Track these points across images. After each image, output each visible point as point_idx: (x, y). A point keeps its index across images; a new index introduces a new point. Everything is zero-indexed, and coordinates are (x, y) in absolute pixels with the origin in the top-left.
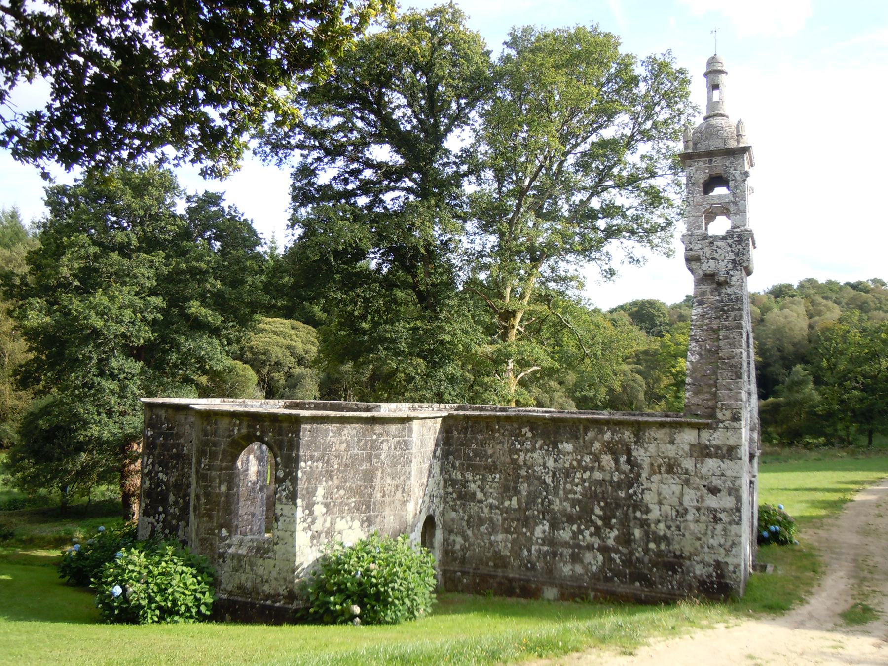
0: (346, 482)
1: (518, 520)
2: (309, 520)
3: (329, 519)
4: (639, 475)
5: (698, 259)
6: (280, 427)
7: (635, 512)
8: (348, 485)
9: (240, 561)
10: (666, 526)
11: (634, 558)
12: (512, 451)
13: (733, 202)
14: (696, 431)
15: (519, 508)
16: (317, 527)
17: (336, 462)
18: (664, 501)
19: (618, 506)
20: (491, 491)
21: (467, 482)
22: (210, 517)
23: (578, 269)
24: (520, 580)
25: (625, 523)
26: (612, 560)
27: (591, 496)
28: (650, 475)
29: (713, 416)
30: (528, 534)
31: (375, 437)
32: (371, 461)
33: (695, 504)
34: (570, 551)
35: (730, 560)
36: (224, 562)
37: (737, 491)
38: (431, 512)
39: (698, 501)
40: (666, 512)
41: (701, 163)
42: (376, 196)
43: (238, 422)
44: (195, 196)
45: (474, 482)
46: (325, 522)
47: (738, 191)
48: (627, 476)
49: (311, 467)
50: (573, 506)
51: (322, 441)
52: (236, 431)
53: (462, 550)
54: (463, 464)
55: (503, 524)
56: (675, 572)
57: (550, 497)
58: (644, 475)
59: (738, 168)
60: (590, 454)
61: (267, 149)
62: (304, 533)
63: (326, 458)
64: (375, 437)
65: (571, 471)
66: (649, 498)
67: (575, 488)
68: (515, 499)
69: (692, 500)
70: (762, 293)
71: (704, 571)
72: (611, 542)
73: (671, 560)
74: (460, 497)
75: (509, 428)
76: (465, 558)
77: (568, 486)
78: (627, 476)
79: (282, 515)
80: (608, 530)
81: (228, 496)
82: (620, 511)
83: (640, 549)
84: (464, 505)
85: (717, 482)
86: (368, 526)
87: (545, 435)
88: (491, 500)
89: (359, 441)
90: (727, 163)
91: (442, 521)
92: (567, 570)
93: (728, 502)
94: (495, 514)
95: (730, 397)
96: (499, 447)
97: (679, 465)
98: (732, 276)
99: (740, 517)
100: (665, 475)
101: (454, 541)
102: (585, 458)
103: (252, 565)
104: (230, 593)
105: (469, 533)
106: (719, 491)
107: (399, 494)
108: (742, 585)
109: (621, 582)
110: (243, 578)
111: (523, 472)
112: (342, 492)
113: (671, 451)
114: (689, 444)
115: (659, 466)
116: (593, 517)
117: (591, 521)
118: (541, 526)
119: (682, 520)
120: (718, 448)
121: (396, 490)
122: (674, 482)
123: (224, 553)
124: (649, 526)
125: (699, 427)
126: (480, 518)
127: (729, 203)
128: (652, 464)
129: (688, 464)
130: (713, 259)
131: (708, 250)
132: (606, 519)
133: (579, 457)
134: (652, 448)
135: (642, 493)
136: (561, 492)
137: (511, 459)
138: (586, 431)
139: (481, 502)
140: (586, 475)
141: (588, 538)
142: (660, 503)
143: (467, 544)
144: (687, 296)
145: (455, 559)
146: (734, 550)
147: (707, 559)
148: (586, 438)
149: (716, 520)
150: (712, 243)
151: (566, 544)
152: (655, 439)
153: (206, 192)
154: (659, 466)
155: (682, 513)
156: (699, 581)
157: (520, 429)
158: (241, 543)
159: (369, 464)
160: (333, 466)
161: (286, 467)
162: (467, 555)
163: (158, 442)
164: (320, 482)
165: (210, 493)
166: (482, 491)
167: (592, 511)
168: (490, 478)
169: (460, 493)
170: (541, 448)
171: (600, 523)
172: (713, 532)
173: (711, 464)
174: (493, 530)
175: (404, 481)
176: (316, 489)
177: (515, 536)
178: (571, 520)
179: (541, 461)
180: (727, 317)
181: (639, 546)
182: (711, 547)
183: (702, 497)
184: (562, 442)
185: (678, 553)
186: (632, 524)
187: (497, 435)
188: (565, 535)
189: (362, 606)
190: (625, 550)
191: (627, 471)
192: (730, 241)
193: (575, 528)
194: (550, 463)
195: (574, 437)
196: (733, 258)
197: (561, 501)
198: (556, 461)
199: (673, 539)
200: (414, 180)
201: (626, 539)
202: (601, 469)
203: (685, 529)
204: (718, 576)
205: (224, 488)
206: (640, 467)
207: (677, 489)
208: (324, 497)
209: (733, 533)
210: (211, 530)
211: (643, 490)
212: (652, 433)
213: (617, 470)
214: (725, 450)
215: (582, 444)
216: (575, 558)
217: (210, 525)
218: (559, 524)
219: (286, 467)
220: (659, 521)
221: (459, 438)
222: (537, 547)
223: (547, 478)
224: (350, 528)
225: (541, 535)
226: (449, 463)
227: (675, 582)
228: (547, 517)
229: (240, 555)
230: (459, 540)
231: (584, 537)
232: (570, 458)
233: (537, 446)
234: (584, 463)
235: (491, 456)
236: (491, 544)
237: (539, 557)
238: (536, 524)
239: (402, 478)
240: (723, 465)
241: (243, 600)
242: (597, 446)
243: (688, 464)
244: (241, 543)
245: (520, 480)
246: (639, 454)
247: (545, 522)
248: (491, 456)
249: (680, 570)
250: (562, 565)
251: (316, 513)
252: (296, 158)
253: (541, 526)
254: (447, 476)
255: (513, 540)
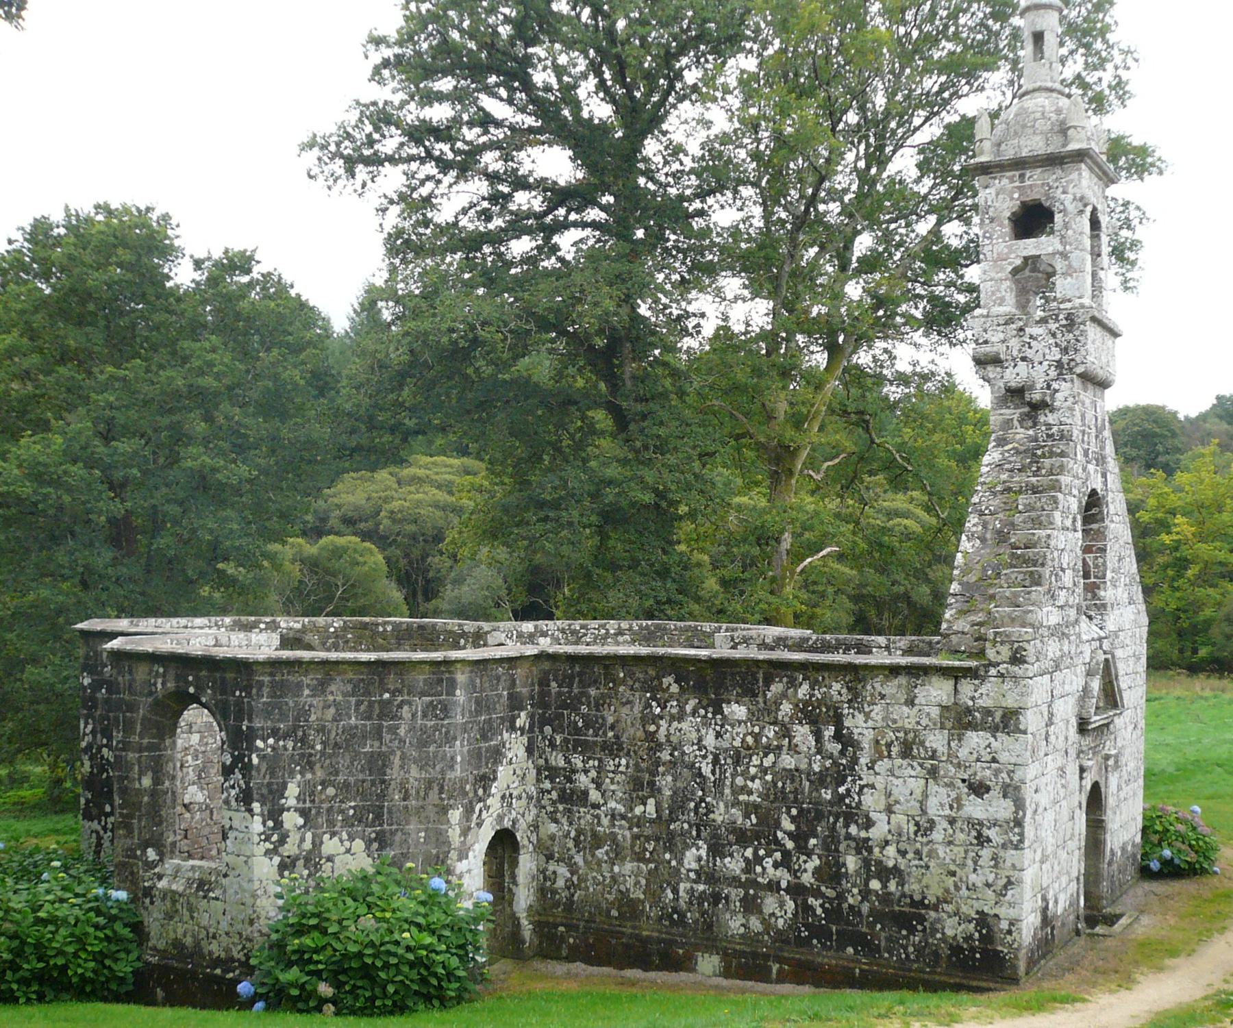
0: (337, 773)
1: (657, 839)
2: (275, 838)
3: (309, 836)
4: (855, 761)
5: (996, 361)
6: (223, 680)
7: (847, 826)
8: (341, 778)
9: (174, 902)
10: (899, 851)
11: (845, 906)
12: (648, 718)
13: (1061, 254)
14: (952, 682)
15: (659, 817)
16: (290, 848)
17: (318, 740)
18: (897, 808)
19: (820, 816)
20: (613, 787)
21: (574, 771)
22: (128, 827)
23: (938, 360)
24: (659, 941)
25: (831, 845)
26: (809, 909)
27: (776, 798)
28: (873, 762)
29: (981, 654)
30: (674, 863)
31: (387, 696)
32: (380, 738)
33: (948, 812)
34: (742, 892)
35: (1002, 911)
36: (152, 903)
37: (1017, 788)
38: (507, 824)
39: (951, 807)
40: (900, 827)
41: (1005, 181)
42: (547, 239)
43: (161, 670)
44: (209, 259)
45: (586, 771)
46: (303, 840)
47: (1070, 232)
48: (835, 763)
49: (274, 749)
50: (747, 816)
51: (291, 704)
52: (159, 686)
53: (569, 888)
54: (566, 741)
55: (633, 846)
56: (912, 931)
57: (708, 799)
58: (863, 761)
59: (1070, 190)
60: (775, 723)
61: (338, 166)
62: (267, 860)
63: (300, 733)
64: (387, 696)
65: (743, 752)
66: (870, 801)
67: (750, 784)
68: (651, 801)
69: (942, 805)
70: (1181, 417)
71: (960, 929)
72: (807, 879)
73: (906, 909)
74: (564, 797)
75: (641, 676)
76: (572, 902)
77: (739, 781)
78: (835, 763)
79: (231, 828)
80: (804, 858)
81: (154, 793)
82: (824, 824)
83: (855, 891)
84: (570, 811)
85: (983, 773)
86: (381, 848)
87: (700, 688)
88: (612, 804)
89: (358, 704)
90: (1051, 180)
91: (534, 838)
92: (735, 924)
93: (1001, 808)
94: (621, 827)
95: (1013, 620)
96: (625, 710)
97: (922, 743)
98: (1056, 391)
99: (1022, 834)
100: (899, 761)
101: (554, 872)
102: (766, 730)
103: (191, 910)
104: (163, 954)
105: (579, 859)
106: (988, 789)
107: (433, 796)
108: (1022, 954)
109: (824, 945)
110: (180, 931)
111: (665, 756)
112: (331, 791)
113: (906, 717)
114: (940, 705)
115: (889, 745)
116: (780, 834)
117: (777, 841)
118: (694, 850)
119: (925, 840)
120: (988, 712)
121: (429, 787)
122: (913, 773)
123: (151, 888)
124: (870, 850)
125: (955, 675)
126: (595, 835)
127: (1053, 254)
128: (877, 742)
129: (937, 740)
130: (1024, 359)
131: (1014, 343)
132: (800, 838)
133: (757, 729)
134: (877, 712)
135: (860, 793)
136: (727, 791)
137: (646, 732)
138: (768, 682)
139: (596, 806)
140: (768, 761)
141: (770, 870)
142: (889, 810)
143: (575, 879)
144: (1218, 398)
145: (557, 904)
146: (1010, 893)
147: (964, 909)
148: (769, 695)
149: (982, 840)
150: (1021, 329)
151: (734, 881)
152: (883, 697)
153: (226, 251)
154: (889, 745)
155: (925, 828)
156: (951, 947)
157: (659, 678)
158: (177, 872)
159: (377, 744)
160: (313, 747)
161: (234, 749)
162: (576, 898)
163: (99, 695)
164: (292, 774)
165: (126, 788)
166: (598, 787)
167: (778, 825)
168: (610, 764)
169: (563, 790)
170: (694, 712)
171: (790, 845)
172: (975, 863)
173: (975, 740)
174: (617, 854)
175: (443, 772)
176: (284, 786)
177: (652, 866)
178: (743, 838)
179: (694, 736)
180: (1039, 469)
181: (854, 886)
182: (972, 888)
183: (958, 799)
184: (729, 702)
185: (917, 897)
186: (842, 848)
187: (621, 689)
188: (733, 865)
189: (338, 985)
190: (830, 893)
191: (836, 753)
192: (1053, 326)
193: (749, 853)
194: (710, 740)
195: (749, 692)
196: (1058, 357)
197: (726, 807)
198: (718, 735)
199: (909, 874)
200: (603, 208)
201: (831, 873)
202: (793, 749)
203: (929, 855)
204: (982, 938)
205: (147, 782)
206: (856, 745)
207: (917, 785)
208: (298, 798)
209: (1008, 864)
210: (131, 850)
211: (862, 788)
212: (877, 685)
213: (819, 752)
214: (998, 716)
215: (762, 705)
216: (750, 906)
217: (129, 841)
218: (723, 846)
219: (234, 749)
220: (887, 843)
221: (559, 694)
222: (688, 885)
223: (703, 765)
224: (348, 851)
225: (694, 866)
226: (544, 738)
227: (911, 949)
228: (703, 834)
229: (174, 892)
230: (563, 871)
231: (764, 869)
232: (741, 730)
233: (689, 708)
234: (764, 740)
235: (612, 728)
236: (614, 879)
237: (691, 903)
238: (687, 847)
239: (438, 768)
240: (995, 744)
241: (181, 965)
242: (786, 707)
243: (937, 740)
244: (177, 872)
245: (661, 769)
246: (856, 724)
247: (701, 843)
248: (612, 728)
249: (920, 928)
250: (728, 916)
251: (287, 825)
252: (392, 179)
253: (694, 850)
254: (541, 762)
255: (650, 872)
